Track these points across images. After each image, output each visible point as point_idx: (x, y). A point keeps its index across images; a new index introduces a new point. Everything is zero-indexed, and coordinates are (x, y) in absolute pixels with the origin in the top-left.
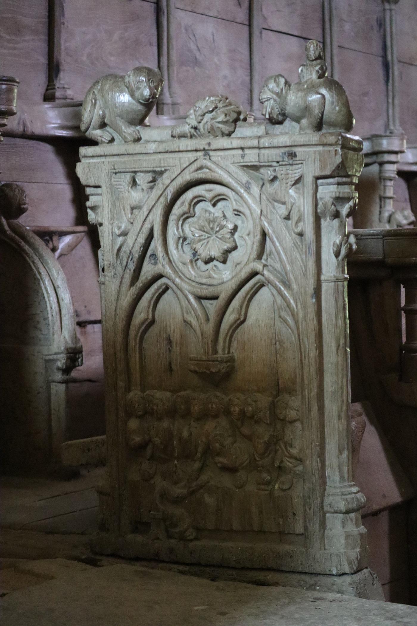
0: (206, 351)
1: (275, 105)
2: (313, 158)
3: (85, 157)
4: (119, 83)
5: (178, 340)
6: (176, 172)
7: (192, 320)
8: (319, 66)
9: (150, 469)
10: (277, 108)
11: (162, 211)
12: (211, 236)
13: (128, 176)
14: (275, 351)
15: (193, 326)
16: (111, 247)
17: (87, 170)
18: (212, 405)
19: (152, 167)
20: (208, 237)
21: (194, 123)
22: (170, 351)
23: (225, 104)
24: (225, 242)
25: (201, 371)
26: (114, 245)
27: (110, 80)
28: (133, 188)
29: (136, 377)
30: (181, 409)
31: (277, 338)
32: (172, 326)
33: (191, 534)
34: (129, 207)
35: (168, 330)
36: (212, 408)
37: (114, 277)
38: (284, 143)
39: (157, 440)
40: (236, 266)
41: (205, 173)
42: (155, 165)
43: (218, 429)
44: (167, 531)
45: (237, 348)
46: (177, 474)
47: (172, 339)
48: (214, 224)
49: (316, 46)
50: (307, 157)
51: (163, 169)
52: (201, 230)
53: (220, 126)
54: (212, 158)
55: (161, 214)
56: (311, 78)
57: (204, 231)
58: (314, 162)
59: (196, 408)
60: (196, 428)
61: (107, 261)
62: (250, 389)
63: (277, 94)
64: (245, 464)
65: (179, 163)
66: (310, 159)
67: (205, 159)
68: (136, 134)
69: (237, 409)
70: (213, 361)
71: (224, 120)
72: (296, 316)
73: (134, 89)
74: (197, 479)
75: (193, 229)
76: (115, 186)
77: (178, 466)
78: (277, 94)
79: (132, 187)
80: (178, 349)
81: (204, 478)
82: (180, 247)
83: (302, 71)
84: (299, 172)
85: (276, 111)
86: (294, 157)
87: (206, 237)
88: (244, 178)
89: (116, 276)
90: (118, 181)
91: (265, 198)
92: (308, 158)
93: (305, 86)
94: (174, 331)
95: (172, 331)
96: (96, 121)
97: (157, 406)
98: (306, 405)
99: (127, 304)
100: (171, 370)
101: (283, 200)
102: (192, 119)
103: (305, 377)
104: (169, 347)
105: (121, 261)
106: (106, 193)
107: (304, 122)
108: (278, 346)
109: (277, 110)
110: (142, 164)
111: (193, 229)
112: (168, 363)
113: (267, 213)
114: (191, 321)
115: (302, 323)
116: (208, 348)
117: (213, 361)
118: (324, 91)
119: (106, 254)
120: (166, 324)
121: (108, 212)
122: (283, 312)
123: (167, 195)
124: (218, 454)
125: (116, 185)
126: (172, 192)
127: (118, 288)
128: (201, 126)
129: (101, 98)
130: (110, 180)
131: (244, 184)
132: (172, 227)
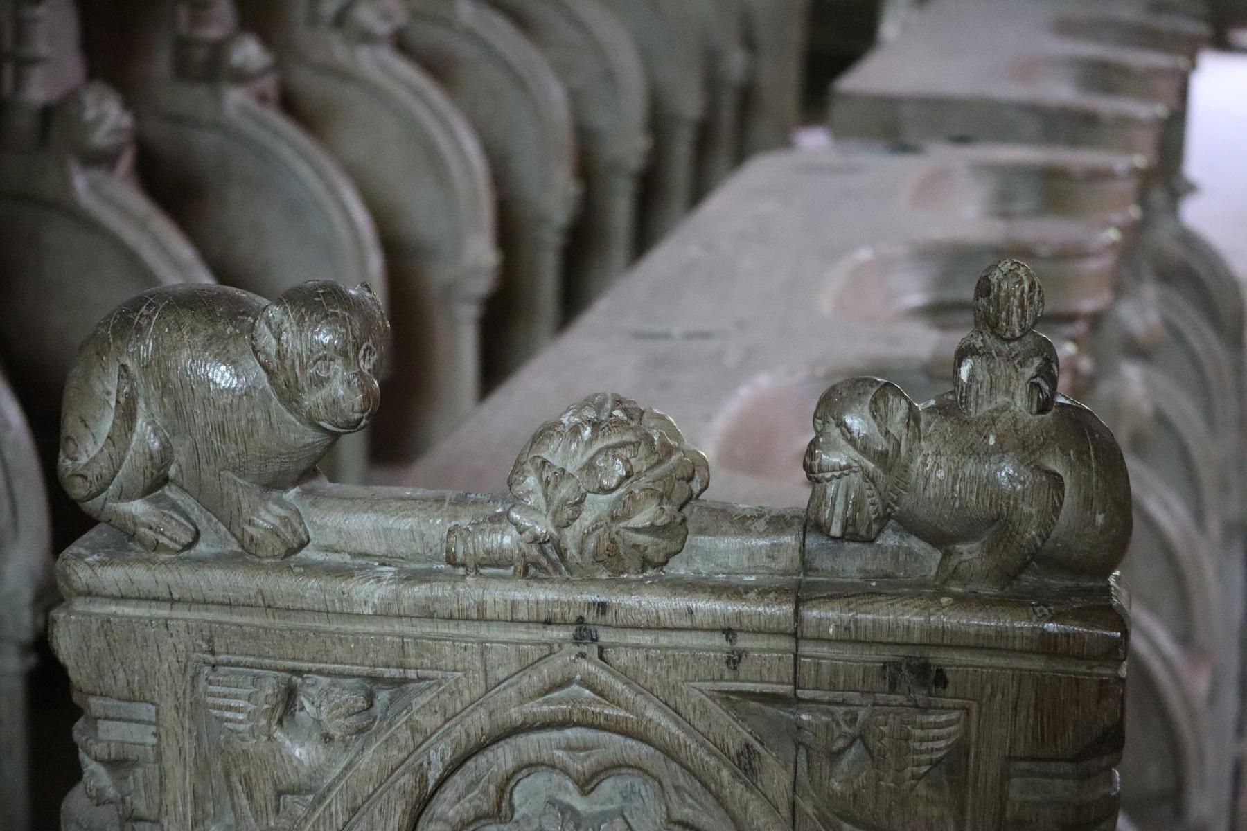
1: (869, 492)
3: (89, 593)
4: (231, 347)
6: (466, 693)
8: (1037, 362)
10: (873, 504)
13: (270, 686)
17: (98, 644)
21: (543, 527)
23: (655, 458)
27: (193, 331)
28: (285, 723)
34: (269, 790)
38: (900, 632)
41: (574, 700)
42: (382, 658)
49: (1030, 291)
50: (988, 690)
53: (642, 539)
54: (610, 654)
56: (1006, 408)
58: (1015, 708)
63: (881, 458)
67: (582, 655)
68: (294, 532)
71: (658, 523)
73: (303, 382)
78: (881, 458)
79: (280, 722)
83: (972, 375)
84: (950, 735)
85: (870, 511)
88: (736, 734)
90: (225, 697)
92: (993, 695)
93: (992, 441)
96: (133, 463)
102: (534, 509)
103: (407, 762)
106: (179, 730)
107: (969, 552)
109: (872, 508)
110: (327, 651)
126: (447, 759)
128: (570, 538)
129: (158, 394)
130: (194, 688)
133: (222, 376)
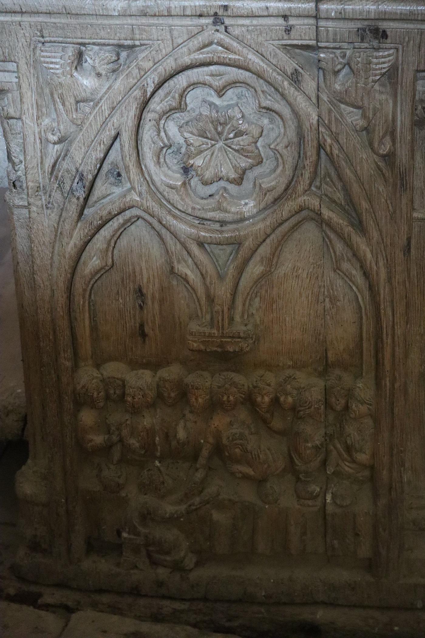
0: (220, 324)
2: (417, 41)
5: (157, 296)
6: (164, 51)
7: (189, 273)
9: (119, 477)
11: (138, 110)
12: (216, 143)
14: (322, 311)
15: (191, 282)
16: (39, 161)
18: (229, 397)
19: (116, 38)
20: (212, 146)
22: (141, 307)
24: (246, 157)
25: (208, 350)
26: (44, 157)
29: (86, 347)
30: (171, 398)
31: (326, 293)
32: (145, 272)
33: (190, 561)
34: (72, 101)
35: (138, 278)
36: (229, 401)
37: (47, 208)
39: (134, 442)
40: (266, 194)
41: (214, 52)
42: (123, 36)
43: (234, 426)
44: (149, 556)
45: (260, 307)
46: (166, 485)
47: (144, 291)
48: (224, 128)
51: (137, 43)
52: (202, 136)
54: (230, 29)
55: (135, 115)
57: (207, 138)
58: (419, 47)
59: (200, 400)
60: (196, 422)
61: (33, 181)
62: (281, 364)
64: (278, 472)
65: (169, 37)
66: (412, 42)
67: (217, 31)
69: (267, 399)
70: (233, 337)
72: (375, 276)
74: (201, 492)
75: (187, 135)
76: (45, 65)
77: (162, 468)
79: (76, 68)
80: (156, 306)
81: (211, 490)
82: (162, 160)
84: (389, 61)
86: (383, 37)
87: (210, 146)
89: (50, 205)
90: (49, 57)
91: (325, 99)
92: (409, 41)
94: (148, 282)
95: (145, 280)
97: (133, 398)
98: (385, 399)
99: (75, 250)
100: (144, 335)
101: (360, 104)
104: (140, 302)
105: (59, 184)
108: (328, 305)
111: (187, 135)
112: (138, 325)
113: (330, 121)
114: (186, 275)
115: (385, 287)
116: (223, 320)
117: (233, 337)
119: (30, 172)
120: (134, 269)
121: (32, 105)
122: (346, 264)
123: (146, 85)
124: (238, 462)
125: (47, 63)
127: (56, 225)
131: (289, 73)
132: (149, 131)
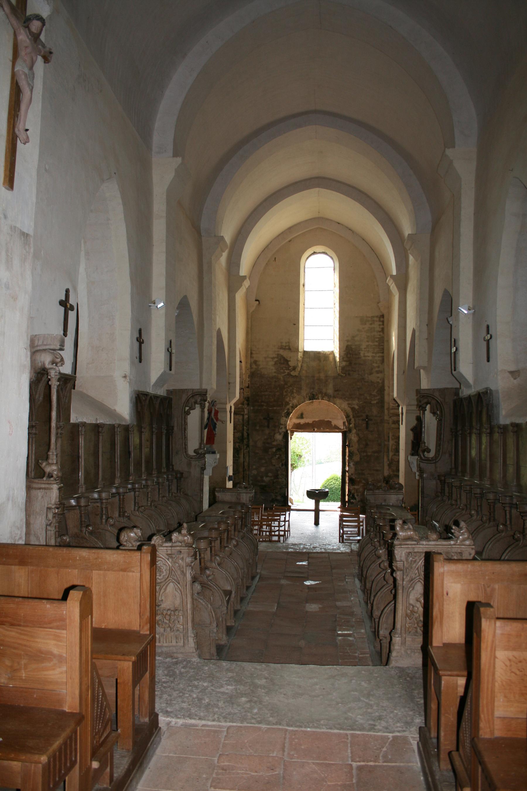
88: (167, 557)
118: (188, 536)
133: (132, 535)
